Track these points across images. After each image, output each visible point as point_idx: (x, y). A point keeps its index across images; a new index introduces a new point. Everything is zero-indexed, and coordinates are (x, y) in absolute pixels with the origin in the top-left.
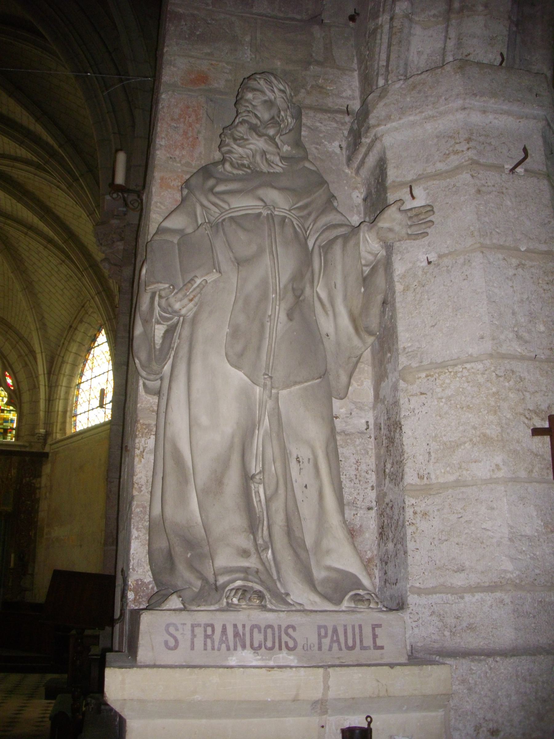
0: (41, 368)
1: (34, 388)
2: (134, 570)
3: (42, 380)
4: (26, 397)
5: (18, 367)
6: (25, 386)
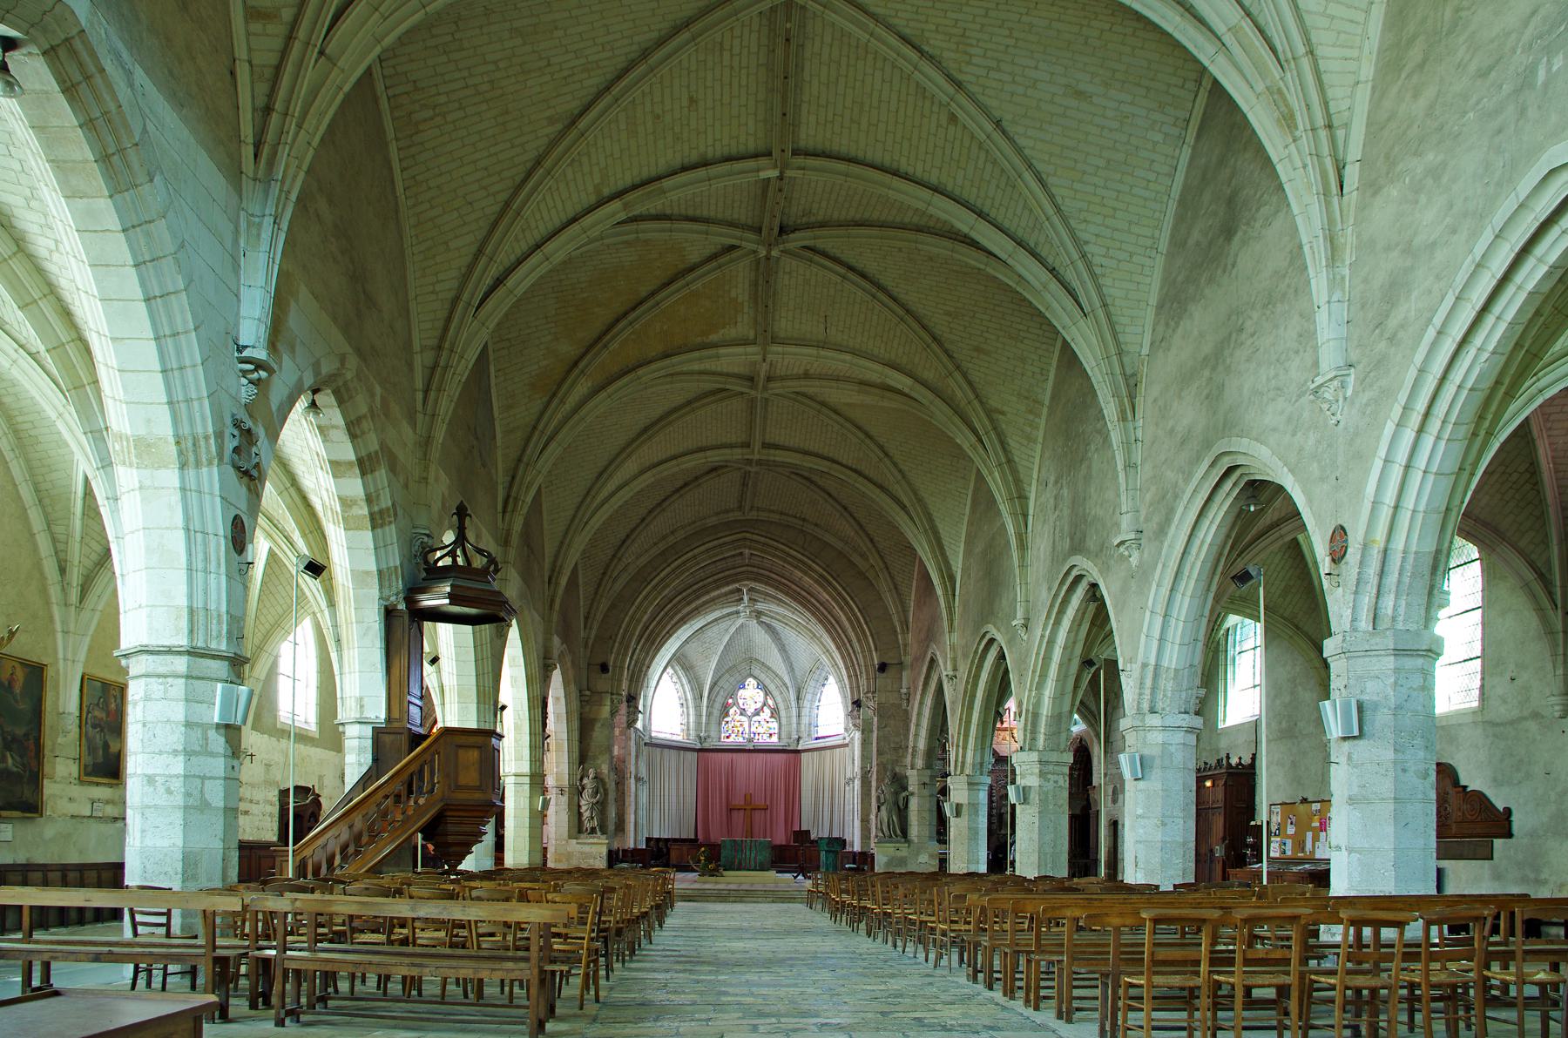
0: (793, 697)
1: (788, 708)
2: (750, 740)
3: (794, 704)
4: (783, 713)
5: (776, 693)
6: (782, 706)
